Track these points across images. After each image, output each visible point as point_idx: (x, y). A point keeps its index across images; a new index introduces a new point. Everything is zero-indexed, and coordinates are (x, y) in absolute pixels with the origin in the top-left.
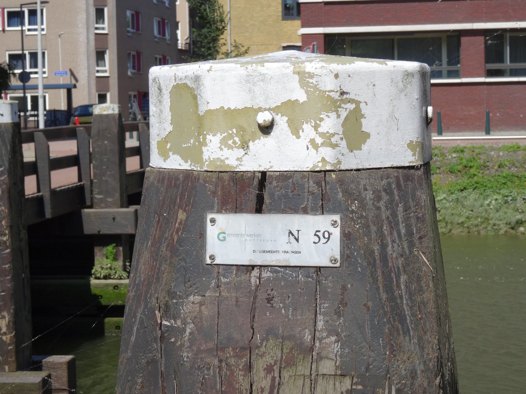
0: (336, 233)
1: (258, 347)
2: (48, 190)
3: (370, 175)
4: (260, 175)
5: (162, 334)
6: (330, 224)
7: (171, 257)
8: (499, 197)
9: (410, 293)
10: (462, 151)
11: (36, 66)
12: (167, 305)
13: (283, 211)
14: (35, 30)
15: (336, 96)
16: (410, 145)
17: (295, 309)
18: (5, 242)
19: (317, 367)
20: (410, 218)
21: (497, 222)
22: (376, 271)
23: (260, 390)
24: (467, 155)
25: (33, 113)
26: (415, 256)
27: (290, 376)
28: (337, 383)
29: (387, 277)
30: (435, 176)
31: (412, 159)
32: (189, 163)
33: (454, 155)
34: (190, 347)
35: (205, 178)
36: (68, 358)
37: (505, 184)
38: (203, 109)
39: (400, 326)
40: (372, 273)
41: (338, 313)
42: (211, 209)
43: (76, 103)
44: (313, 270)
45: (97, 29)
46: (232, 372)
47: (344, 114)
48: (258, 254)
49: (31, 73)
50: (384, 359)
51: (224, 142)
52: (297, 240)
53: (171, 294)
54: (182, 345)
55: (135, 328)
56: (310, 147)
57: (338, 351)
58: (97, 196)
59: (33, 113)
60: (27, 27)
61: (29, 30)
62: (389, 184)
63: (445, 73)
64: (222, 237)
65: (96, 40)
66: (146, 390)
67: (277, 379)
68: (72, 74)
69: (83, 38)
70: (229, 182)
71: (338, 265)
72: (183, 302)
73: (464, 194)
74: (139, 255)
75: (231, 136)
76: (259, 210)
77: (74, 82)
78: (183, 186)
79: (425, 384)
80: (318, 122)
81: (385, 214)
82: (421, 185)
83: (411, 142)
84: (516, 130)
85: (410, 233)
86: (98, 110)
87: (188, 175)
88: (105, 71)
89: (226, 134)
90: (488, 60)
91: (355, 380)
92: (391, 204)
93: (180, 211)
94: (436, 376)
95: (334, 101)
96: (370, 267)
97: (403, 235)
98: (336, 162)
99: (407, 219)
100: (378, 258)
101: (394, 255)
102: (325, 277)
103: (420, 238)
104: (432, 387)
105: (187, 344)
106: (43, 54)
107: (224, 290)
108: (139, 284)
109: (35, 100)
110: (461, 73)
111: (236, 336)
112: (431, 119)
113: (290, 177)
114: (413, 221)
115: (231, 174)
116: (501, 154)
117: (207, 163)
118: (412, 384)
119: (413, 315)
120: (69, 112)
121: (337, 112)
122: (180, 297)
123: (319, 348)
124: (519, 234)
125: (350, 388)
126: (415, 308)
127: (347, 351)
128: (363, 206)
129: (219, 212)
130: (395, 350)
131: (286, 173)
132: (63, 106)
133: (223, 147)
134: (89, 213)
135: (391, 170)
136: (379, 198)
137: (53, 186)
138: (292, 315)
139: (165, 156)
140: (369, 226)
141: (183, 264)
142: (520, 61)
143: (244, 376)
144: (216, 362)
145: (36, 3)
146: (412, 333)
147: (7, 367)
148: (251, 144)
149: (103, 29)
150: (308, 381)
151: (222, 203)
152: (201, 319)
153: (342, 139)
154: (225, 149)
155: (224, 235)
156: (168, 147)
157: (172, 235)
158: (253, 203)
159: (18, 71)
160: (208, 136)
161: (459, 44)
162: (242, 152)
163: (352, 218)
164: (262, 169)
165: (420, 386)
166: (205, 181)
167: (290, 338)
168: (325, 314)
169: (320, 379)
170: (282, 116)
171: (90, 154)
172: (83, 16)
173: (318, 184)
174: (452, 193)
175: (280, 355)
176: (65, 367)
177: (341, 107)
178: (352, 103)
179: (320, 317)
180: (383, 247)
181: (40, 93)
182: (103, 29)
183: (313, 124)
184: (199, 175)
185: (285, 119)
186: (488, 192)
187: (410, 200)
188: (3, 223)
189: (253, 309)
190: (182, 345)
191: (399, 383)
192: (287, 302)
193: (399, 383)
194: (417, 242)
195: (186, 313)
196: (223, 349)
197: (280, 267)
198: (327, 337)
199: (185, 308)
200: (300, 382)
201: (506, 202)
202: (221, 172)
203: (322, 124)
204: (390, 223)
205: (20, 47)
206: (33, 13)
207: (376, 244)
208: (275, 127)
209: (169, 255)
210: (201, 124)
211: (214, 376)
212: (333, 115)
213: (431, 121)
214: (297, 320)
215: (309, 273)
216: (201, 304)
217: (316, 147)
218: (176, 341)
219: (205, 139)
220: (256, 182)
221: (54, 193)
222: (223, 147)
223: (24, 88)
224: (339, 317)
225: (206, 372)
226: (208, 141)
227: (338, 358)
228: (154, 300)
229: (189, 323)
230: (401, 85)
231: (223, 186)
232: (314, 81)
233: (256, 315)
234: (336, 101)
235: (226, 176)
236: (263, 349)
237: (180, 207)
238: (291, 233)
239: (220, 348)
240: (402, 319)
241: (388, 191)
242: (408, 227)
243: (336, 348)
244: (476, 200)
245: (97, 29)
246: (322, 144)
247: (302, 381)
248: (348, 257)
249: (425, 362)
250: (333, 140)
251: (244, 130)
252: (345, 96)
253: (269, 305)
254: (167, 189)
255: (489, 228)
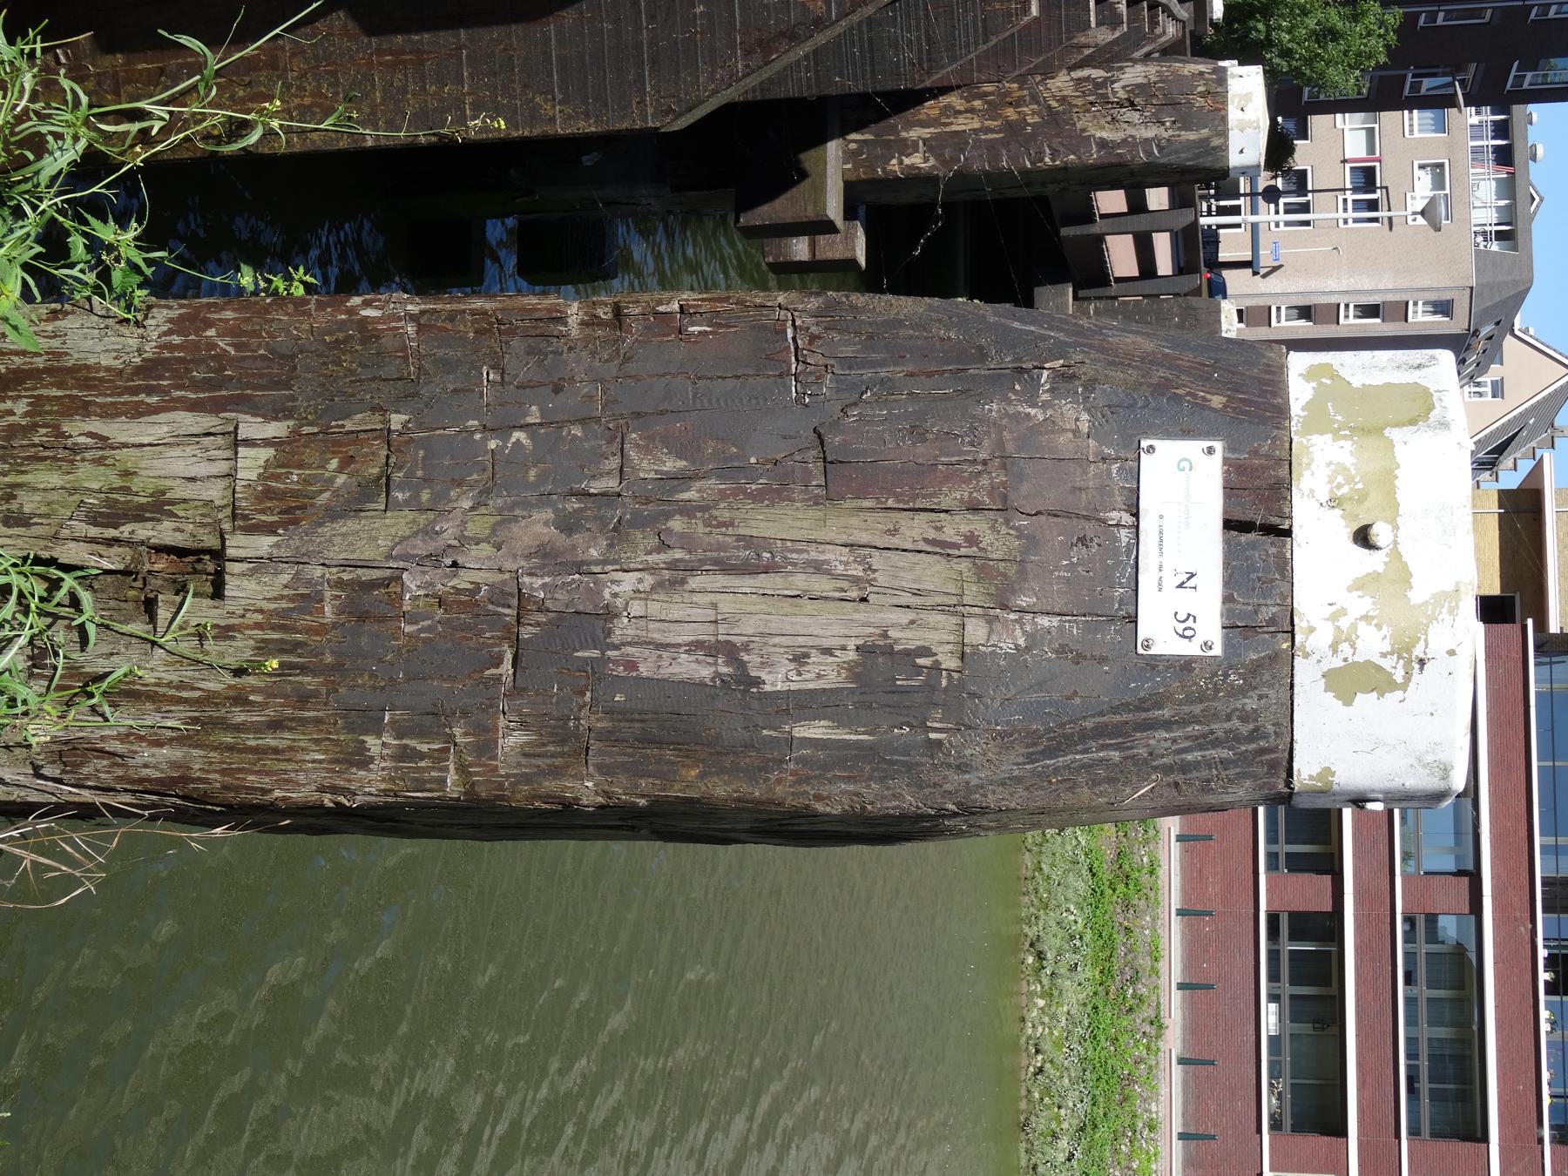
0: (1191, 649)
1: (1007, 522)
2: (1104, 230)
3: (1282, 704)
4: (1286, 527)
5: (1027, 371)
6: (1205, 639)
7: (1150, 385)
8: (1080, 926)
9: (1090, 766)
10: (1152, 873)
11: (1286, 212)
12: (1073, 377)
13: (1227, 564)
14: (1345, 210)
15: (1418, 652)
16: (1328, 771)
17: (1068, 580)
18: (1041, 160)
19: (975, 616)
20: (1210, 768)
21: (1041, 923)
22: (1130, 711)
23: (938, 524)
24: (1145, 879)
25: (1214, 208)
26: (1149, 774)
27: (961, 573)
28: (950, 647)
29: (1119, 730)
30: (1114, 829)
31: (1305, 775)
32: (1303, 414)
33: (1145, 859)
34: (1007, 413)
35: (1280, 439)
36: (862, 261)
37: (1100, 936)
38: (1394, 434)
39: (1040, 748)
40: (1128, 704)
41: (1062, 650)
42: (1230, 448)
43: (1227, 274)
44: (1131, 610)
45: (1347, 306)
46: (967, 481)
47: (1387, 664)
48: (1157, 522)
49: (1277, 205)
50: (989, 723)
51: (1341, 469)
52: (1181, 586)
53: (1090, 385)
54: (1009, 402)
55: (1032, 328)
56: (1334, 608)
57: (1001, 648)
58: (1092, 307)
59: (1214, 208)
60: (1350, 196)
61: (1345, 201)
62: (1265, 737)
63: (1274, 848)
64: (1185, 465)
65: (1329, 305)
66: (938, 344)
67: (957, 552)
68: (1275, 269)
69: (1332, 284)
70: (1275, 477)
71: (1140, 651)
72: (1079, 404)
73: (1085, 872)
74: (1148, 335)
75: (1350, 480)
76: (1229, 525)
77: (1262, 271)
78: (1264, 403)
79: (948, 787)
80: (1375, 622)
81: (1219, 728)
82: (1261, 788)
83: (1333, 774)
84: (1182, 956)
85: (1185, 768)
86: (1228, 309)
87: (1282, 412)
88: (1279, 322)
89: (1353, 472)
90: (1293, 916)
91: (956, 675)
92: (1233, 739)
93: (1224, 400)
94: (958, 804)
95: (1409, 649)
96: (1136, 703)
97: (1184, 756)
98: (1308, 649)
99: (1209, 764)
100: (1150, 714)
101: (1152, 742)
102: (1120, 630)
103: (1177, 785)
104: (943, 797)
105: (1011, 410)
106: (1307, 223)
107: (1098, 468)
108: (1102, 334)
109: (1235, 211)
110: (1274, 874)
111: (1024, 488)
112: (1363, 807)
113: (1283, 577)
114: (1205, 774)
115: (1287, 481)
116: (1147, 932)
117: (1305, 441)
118: (949, 766)
119: (1057, 770)
120: (1216, 265)
121: (1392, 653)
122: (1086, 399)
123: (1006, 620)
124: (1022, 956)
125: (943, 666)
126: (1067, 775)
127: (1002, 663)
128: (1235, 692)
129: (1226, 461)
130: (1003, 739)
131: (1289, 568)
132: (1224, 256)
133: (1332, 467)
134: (1066, 295)
135: (1289, 740)
136: (1244, 719)
137: (1108, 238)
138: (1059, 577)
139: (1310, 374)
140: (1201, 701)
141: (1140, 404)
142: (1291, 967)
143: (962, 499)
144: (983, 456)
145: (1389, 210)
146: (1027, 767)
147: (849, 166)
148: (1338, 512)
149: (1347, 317)
150: (954, 600)
151: (1240, 466)
152: (1053, 432)
153: (1345, 660)
154: (1328, 471)
155: (1187, 468)
156: (1324, 380)
157: (1185, 386)
158: (1239, 516)
159: (1280, 183)
160: (1350, 442)
161: (1320, 872)
162: (1324, 498)
163: (1215, 674)
164: (1295, 530)
165: (945, 777)
166: (1274, 439)
167: (1023, 574)
168: (1060, 628)
169: (955, 620)
170: (1386, 563)
171: (1158, 296)
172: (1366, 283)
173: (1272, 621)
174: (1086, 854)
175: (995, 556)
176: (848, 255)
177: (1399, 658)
178: (1404, 677)
179: (1055, 621)
180: (1167, 725)
181: (1245, 217)
182: (1347, 317)
183: (1371, 614)
184: (1284, 428)
185: (1381, 569)
186: (1088, 910)
187: (1238, 770)
188: (1072, 157)
189: (1068, 515)
190: (1009, 402)
191: (951, 744)
192: (1080, 569)
193: (951, 744)
194: (1170, 779)
195: (1060, 408)
196: (1004, 467)
197: (1137, 557)
198: (1024, 633)
199: (1069, 406)
200: (952, 589)
201: (1072, 937)
202: (1290, 465)
203: (1372, 628)
204: (1204, 736)
205: (1316, 188)
206: (1373, 205)
207: (1173, 713)
208: (1366, 551)
209: (1152, 381)
210: (1369, 431)
211: (961, 453)
212: (1387, 647)
213: (1358, 807)
214: (1051, 584)
215: (1127, 604)
216: (1076, 432)
217: (1334, 618)
218: (1016, 392)
219: (1345, 437)
220: (1274, 520)
221: (1099, 240)
222: (1332, 467)
223: (1253, 194)
224: (1057, 652)
225: (967, 439)
226: (1342, 442)
227: (990, 649)
228: (1079, 358)
229: (1044, 413)
230: (1429, 758)
231: (1267, 468)
232: (1445, 615)
233: (1059, 520)
234: (1409, 651)
235: (1283, 472)
236: (1004, 530)
237: (1231, 399)
238: (1192, 575)
239: (1005, 461)
240: (1050, 753)
241: (1256, 735)
242: (1196, 765)
243: (1007, 646)
244: (1076, 890)
245: (1347, 306)
246: (1338, 627)
247: (953, 591)
248: (1153, 668)
249: (982, 787)
250: (1345, 647)
251: (1360, 501)
252: (1417, 666)
253: (1075, 541)
254: (1256, 378)
255: (1032, 910)
